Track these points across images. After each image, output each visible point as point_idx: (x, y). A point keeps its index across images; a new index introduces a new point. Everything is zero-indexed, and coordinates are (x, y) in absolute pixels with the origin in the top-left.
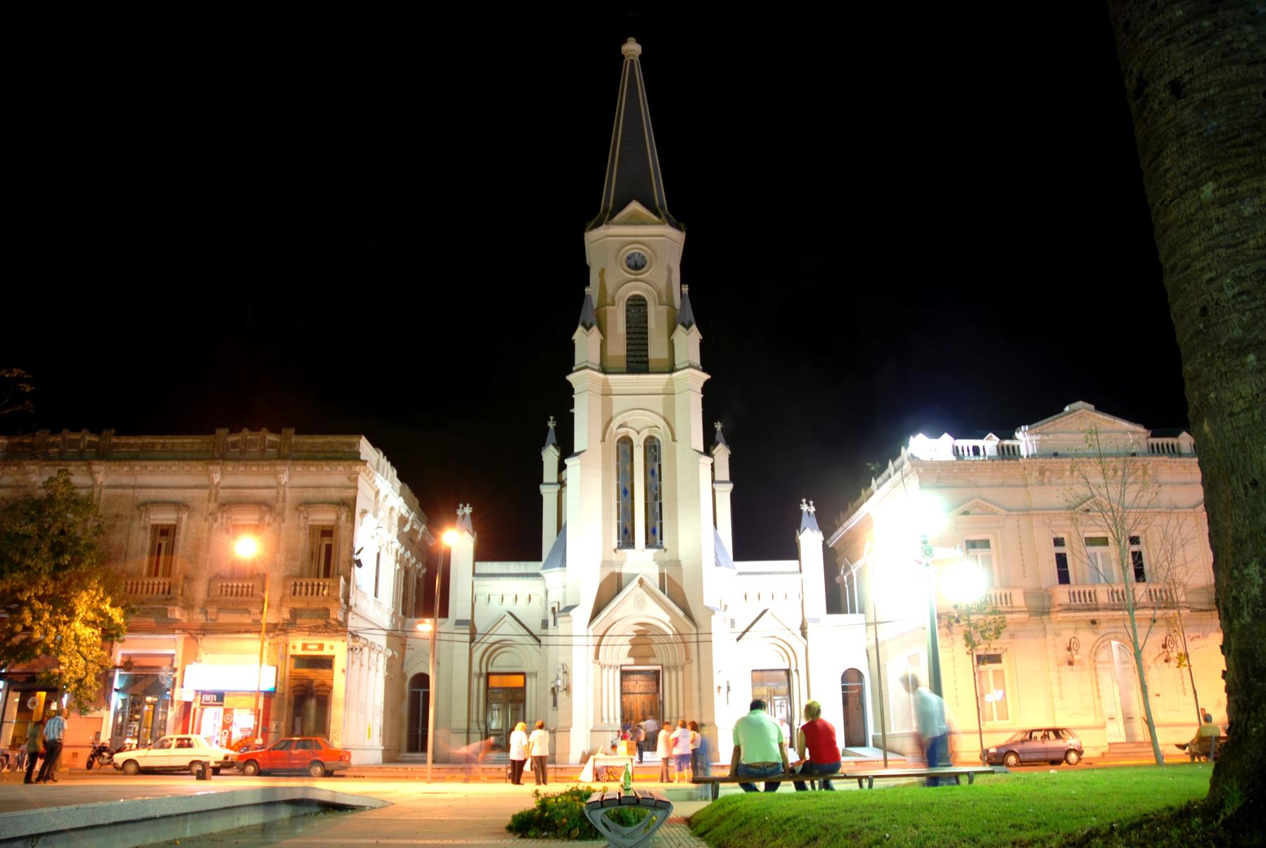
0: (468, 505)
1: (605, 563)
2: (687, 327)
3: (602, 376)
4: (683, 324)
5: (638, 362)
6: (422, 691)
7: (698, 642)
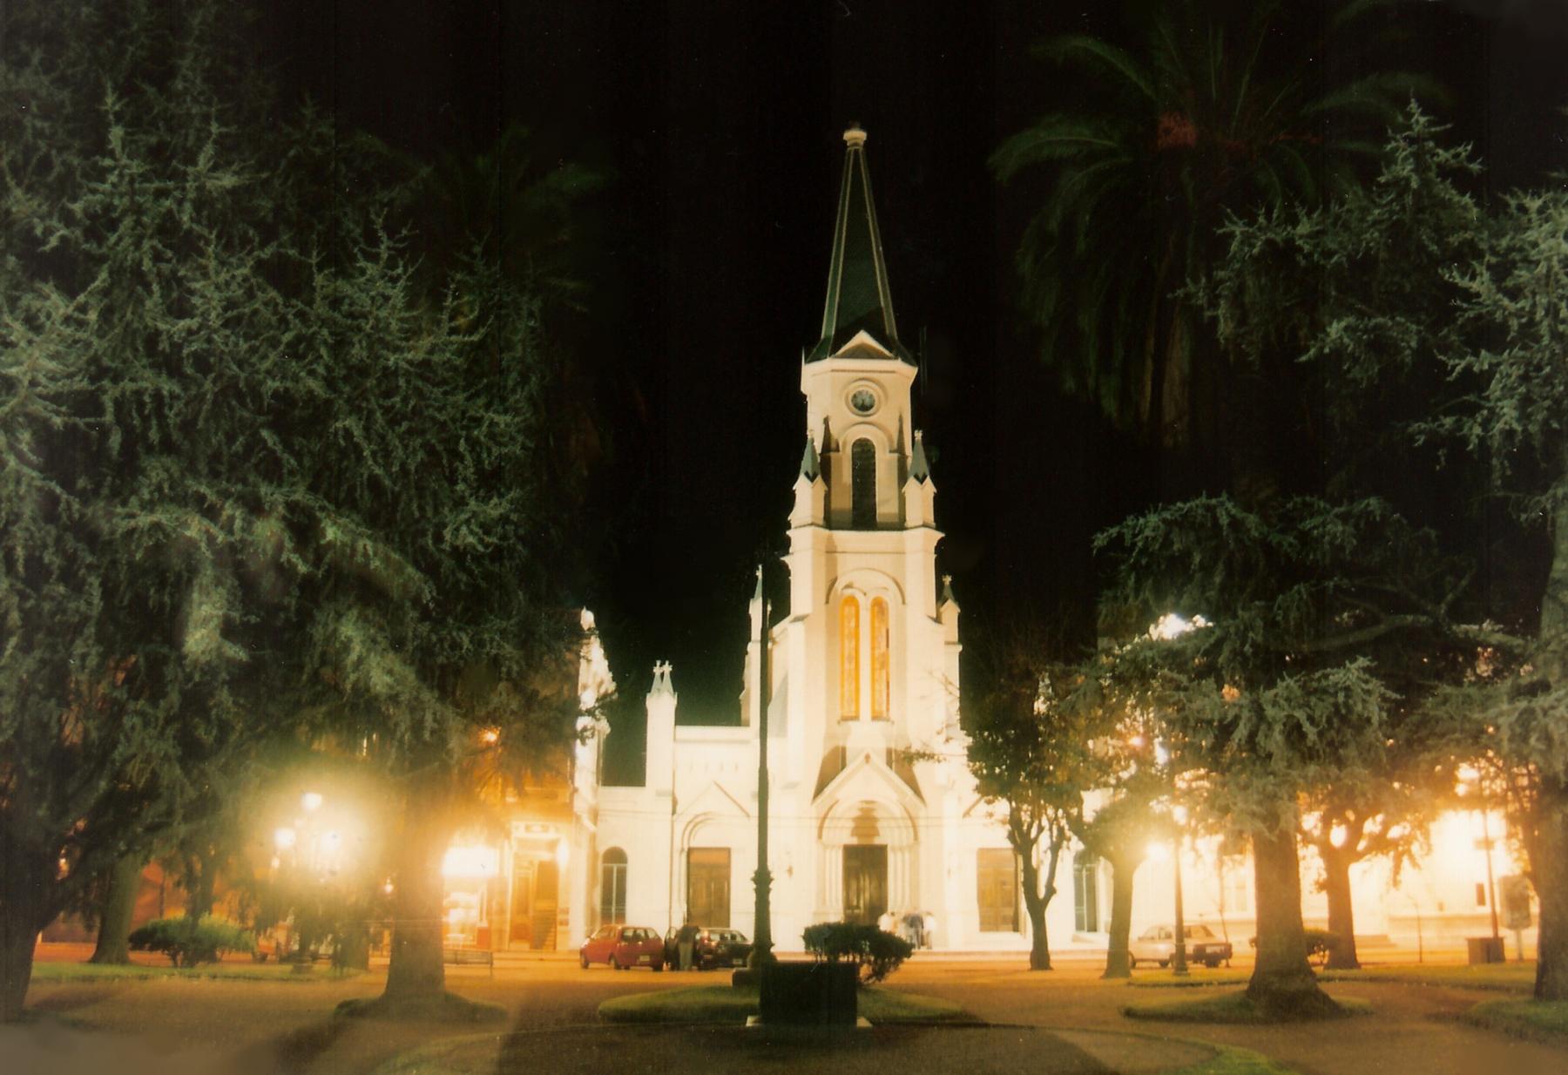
0: (667, 663)
1: (829, 736)
2: (921, 480)
3: (827, 532)
4: (916, 477)
5: (863, 516)
6: (615, 867)
7: (928, 818)
